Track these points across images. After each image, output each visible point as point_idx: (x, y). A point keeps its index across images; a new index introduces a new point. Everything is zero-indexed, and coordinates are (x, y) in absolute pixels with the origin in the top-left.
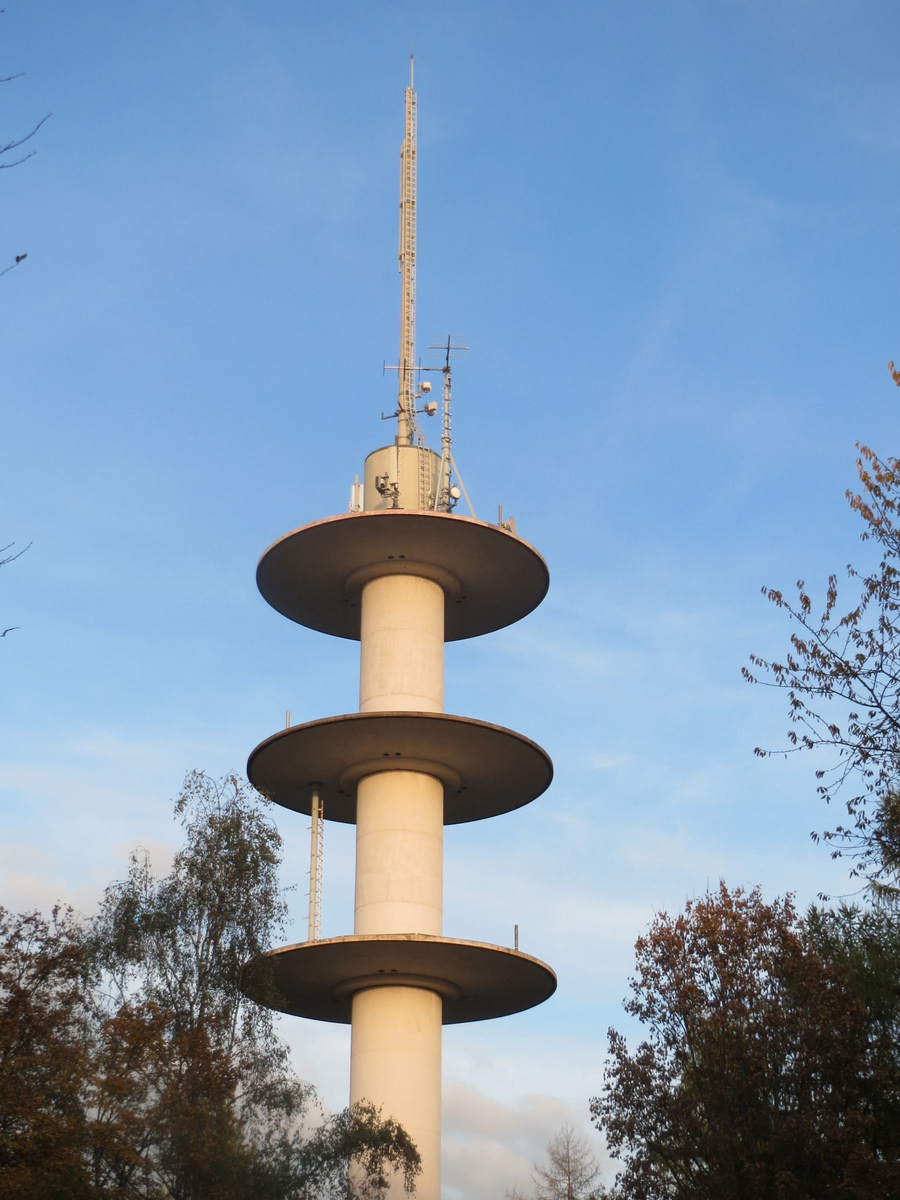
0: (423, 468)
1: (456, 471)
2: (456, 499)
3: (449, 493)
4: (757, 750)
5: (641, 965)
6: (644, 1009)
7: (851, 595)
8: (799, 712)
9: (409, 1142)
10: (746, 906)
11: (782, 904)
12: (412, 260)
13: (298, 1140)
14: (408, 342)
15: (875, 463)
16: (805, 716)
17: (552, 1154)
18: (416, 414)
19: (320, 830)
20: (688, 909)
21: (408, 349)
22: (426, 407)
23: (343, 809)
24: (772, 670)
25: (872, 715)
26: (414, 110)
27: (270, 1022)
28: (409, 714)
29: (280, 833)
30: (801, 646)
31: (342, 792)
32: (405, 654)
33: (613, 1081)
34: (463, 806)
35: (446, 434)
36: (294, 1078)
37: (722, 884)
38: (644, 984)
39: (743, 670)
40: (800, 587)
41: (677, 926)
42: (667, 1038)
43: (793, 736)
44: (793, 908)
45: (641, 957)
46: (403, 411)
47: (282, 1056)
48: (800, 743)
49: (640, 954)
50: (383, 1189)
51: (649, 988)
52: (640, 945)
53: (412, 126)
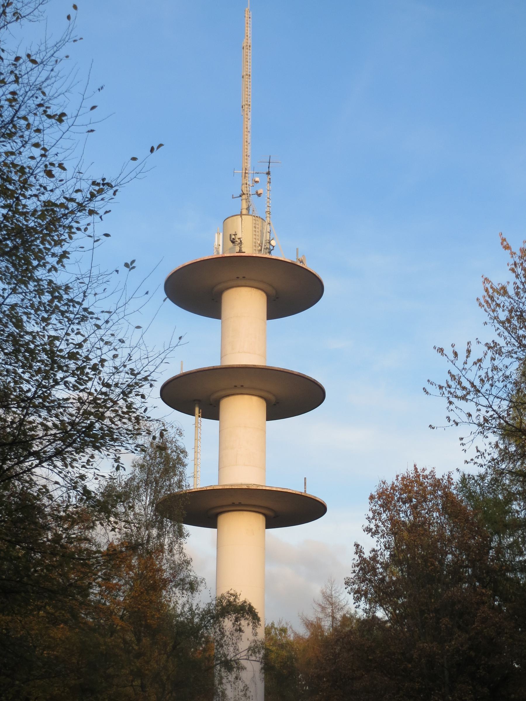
0: (255, 227)
1: (273, 230)
2: (274, 247)
3: (269, 243)
4: (430, 426)
5: (372, 508)
6: (373, 530)
7: (478, 351)
8: (452, 407)
9: (254, 611)
10: (427, 478)
11: (446, 477)
12: (249, 108)
13: (198, 608)
14: (247, 155)
15: (491, 285)
16: (455, 409)
17: (323, 593)
18: (251, 196)
19: (199, 426)
20: (397, 479)
21: (247, 159)
22: (257, 192)
23: (212, 411)
24: (438, 388)
25: (487, 412)
26: (250, 21)
27: (182, 546)
28: (248, 366)
29: (187, 450)
30: (453, 377)
31: (211, 405)
32: (247, 333)
33: (357, 569)
34: (277, 410)
35: (267, 209)
36: (194, 575)
37: (415, 466)
38: (373, 518)
39: (424, 388)
40: (453, 347)
41: (391, 488)
42: (385, 546)
43: (448, 418)
44: (452, 479)
45: (372, 504)
46: (244, 194)
47: (188, 563)
48: (452, 422)
49: (372, 503)
50: (241, 633)
51: (376, 520)
52: (372, 498)
53: (249, 31)
